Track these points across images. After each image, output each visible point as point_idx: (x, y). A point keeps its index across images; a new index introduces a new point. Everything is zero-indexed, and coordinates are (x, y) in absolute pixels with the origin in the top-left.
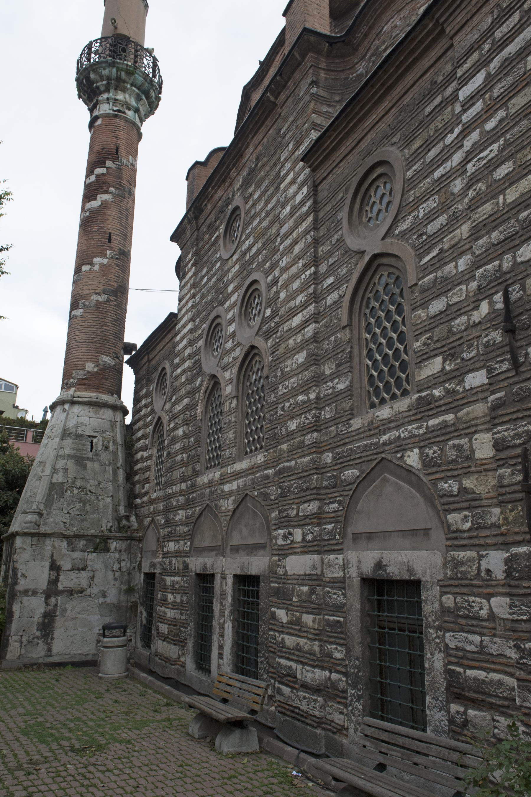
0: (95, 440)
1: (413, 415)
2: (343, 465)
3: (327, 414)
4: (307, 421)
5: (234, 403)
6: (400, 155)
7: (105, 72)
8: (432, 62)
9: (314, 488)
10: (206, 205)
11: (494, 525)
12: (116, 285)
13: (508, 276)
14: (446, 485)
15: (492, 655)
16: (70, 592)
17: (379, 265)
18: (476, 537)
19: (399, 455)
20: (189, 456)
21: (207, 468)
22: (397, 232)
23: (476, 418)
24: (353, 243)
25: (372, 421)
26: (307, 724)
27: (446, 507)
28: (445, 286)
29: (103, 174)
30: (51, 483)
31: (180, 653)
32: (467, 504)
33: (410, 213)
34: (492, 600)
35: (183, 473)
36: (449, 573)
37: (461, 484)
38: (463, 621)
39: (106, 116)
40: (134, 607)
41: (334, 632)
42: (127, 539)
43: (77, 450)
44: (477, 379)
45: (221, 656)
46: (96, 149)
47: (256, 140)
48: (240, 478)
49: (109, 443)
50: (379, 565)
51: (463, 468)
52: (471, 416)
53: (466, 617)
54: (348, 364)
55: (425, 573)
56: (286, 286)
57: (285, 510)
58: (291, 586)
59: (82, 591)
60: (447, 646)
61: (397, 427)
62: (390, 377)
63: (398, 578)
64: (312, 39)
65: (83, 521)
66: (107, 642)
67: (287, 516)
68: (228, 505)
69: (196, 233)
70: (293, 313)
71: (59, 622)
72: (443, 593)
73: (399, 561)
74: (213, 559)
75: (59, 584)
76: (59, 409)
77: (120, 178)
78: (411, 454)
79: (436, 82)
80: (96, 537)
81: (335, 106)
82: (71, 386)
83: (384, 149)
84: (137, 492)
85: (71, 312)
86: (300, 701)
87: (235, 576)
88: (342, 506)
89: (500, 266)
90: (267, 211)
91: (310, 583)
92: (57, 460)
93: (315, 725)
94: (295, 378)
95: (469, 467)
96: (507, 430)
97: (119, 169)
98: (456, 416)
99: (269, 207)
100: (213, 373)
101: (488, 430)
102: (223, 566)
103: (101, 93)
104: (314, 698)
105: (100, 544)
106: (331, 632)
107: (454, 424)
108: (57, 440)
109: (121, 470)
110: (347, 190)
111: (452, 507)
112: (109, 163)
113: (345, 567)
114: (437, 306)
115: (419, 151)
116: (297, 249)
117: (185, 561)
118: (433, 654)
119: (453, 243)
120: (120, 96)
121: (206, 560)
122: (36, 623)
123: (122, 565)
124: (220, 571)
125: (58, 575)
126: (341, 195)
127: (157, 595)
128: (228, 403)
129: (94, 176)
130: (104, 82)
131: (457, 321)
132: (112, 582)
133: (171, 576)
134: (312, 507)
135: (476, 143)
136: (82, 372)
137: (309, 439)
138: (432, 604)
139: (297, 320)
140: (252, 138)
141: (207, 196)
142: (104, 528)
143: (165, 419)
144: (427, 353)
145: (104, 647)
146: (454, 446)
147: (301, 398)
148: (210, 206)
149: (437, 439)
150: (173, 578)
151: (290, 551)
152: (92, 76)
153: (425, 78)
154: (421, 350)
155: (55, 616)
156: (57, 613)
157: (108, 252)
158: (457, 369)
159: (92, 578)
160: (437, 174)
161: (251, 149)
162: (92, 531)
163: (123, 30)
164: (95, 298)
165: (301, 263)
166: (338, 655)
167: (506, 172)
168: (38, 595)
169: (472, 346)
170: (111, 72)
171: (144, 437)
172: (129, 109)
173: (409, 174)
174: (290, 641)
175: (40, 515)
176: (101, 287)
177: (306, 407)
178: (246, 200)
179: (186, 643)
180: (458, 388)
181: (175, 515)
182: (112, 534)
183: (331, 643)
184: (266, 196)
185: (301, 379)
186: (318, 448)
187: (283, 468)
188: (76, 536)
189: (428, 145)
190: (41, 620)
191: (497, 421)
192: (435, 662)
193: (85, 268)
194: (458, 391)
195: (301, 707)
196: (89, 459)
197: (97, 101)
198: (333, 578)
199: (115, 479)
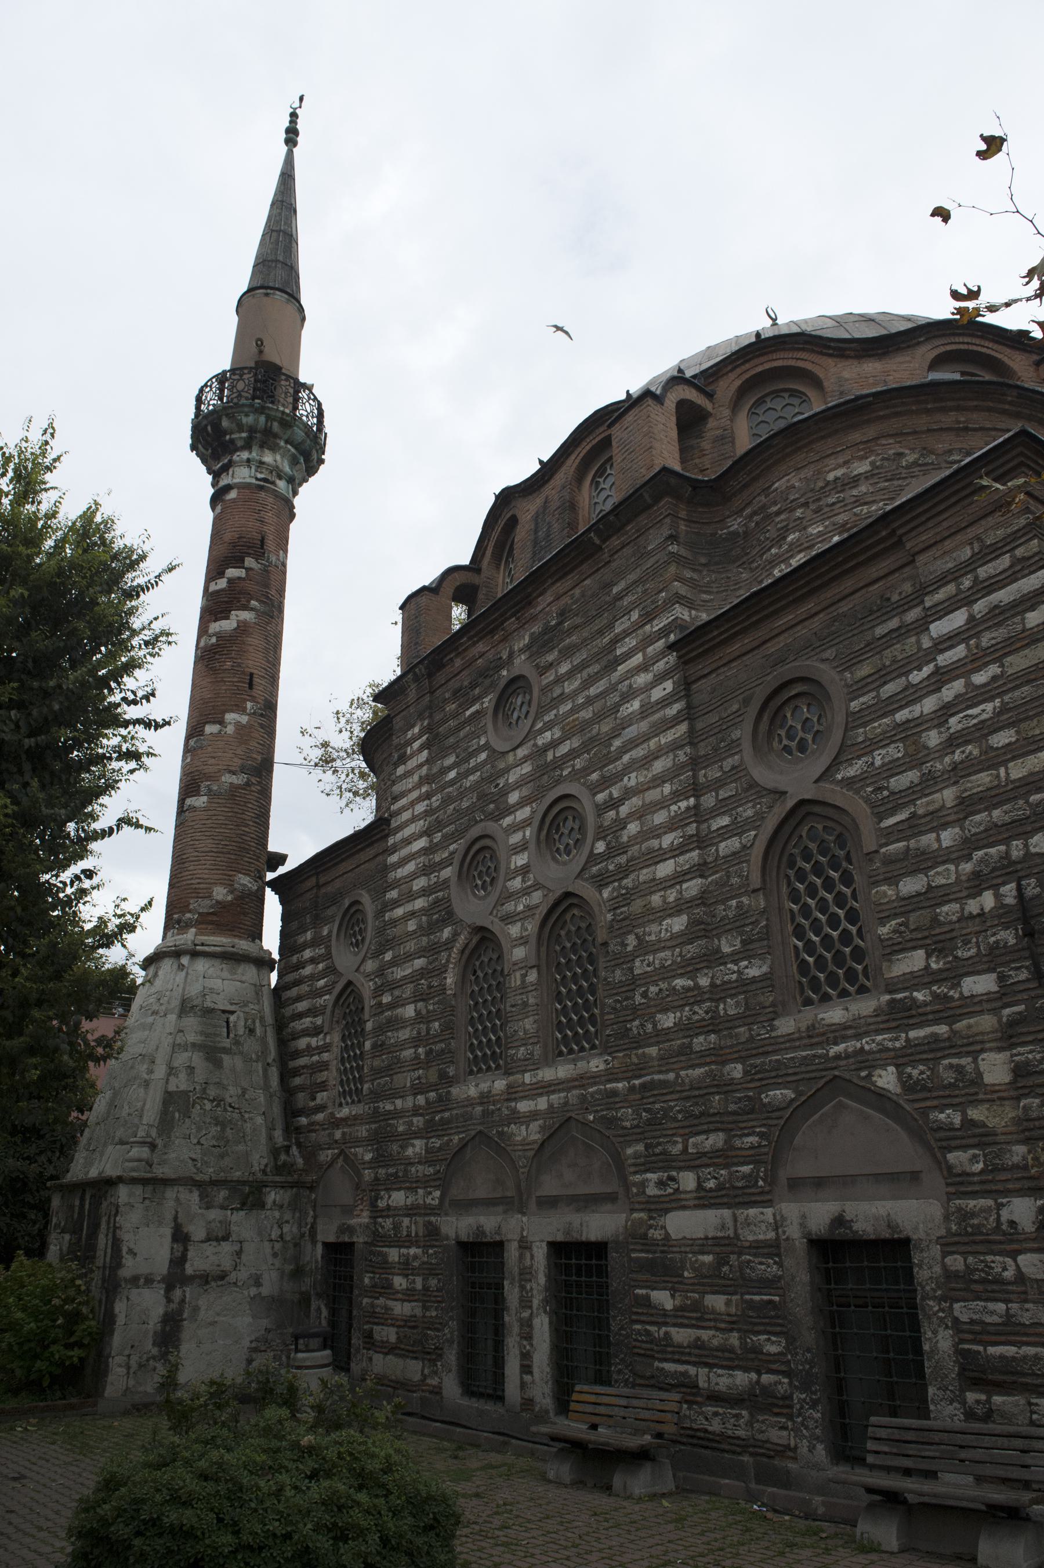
0: (232, 1018)
1: (883, 1022)
2: (764, 1082)
3: (730, 1007)
4: (696, 1017)
5: (532, 976)
6: (837, 678)
7: (248, 420)
8: (882, 573)
9: (715, 1114)
10: (451, 659)
11: (1016, 1167)
12: (259, 758)
13: (1019, 867)
14: (942, 1116)
15: (1024, 1325)
16: (205, 1279)
17: (808, 814)
18: (991, 1181)
19: (863, 1074)
20: (428, 1053)
21: (471, 1073)
22: (839, 777)
23: (982, 1033)
24: (764, 775)
25: (813, 1025)
26: (723, 1451)
27: (944, 1144)
28: (923, 862)
29: (239, 578)
30: (167, 1092)
31: (426, 1371)
32: (976, 1140)
33: (859, 757)
34: (1020, 1258)
35: (419, 1078)
36: (954, 1228)
37: (964, 1114)
38: (979, 1287)
39: (243, 487)
40: (305, 1300)
41: (770, 1317)
42: (292, 1185)
43: (207, 1035)
44: (980, 984)
45: (526, 1369)
46: (228, 537)
47: (560, 587)
48: (554, 1092)
49: (254, 1022)
50: (839, 1221)
51: (967, 1094)
52: (975, 1030)
53: (983, 1281)
54: (765, 943)
55: (916, 1228)
56: (639, 814)
57: (659, 1144)
58: (678, 1256)
59: (223, 1276)
60: (956, 1320)
61: (858, 1037)
62: (837, 965)
63: (872, 1237)
64: (673, 481)
65: (222, 1156)
66: (304, 1359)
67: (664, 1153)
68: (531, 1133)
69: (427, 698)
70: (659, 856)
71: (188, 1330)
72: (945, 1254)
73: (870, 1214)
74: (499, 1218)
75: (187, 1266)
76: (167, 966)
77: (267, 586)
78: (883, 1073)
79: (889, 599)
80: (244, 1183)
81: (700, 572)
82: (188, 925)
83: (807, 663)
84: (300, 1104)
85: (181, 802)
86: (707, 1419)
87: (552, 1245)
88: (767, 1139)
89: (1007, 853)
90: (588, 697)
91: (717, 1249)
92: (173, 1052)
93: (739, 1450)
94: (668, 953)
95: (976, 1094)
96: (1031, 1052)
97: (266, 571)
98: (951, 1030)
99: (593, 691)
100: (479, 923)
101: (1000, 1050)
102: (523, 1229)
103: (237, 450)
104: (734, 1412)
105: (249, 1196)
106: (759, 1317)
107: (949, 1038)
108: (172, 1017)
109: (274, 1069)
110: (746, 702)
111: (953, 1143)
112: (249, 562)
113: (777, 1225)
114: (911, 886)
115: (869, 680)
116: (659, 766)
117: (430, 1223)
118: (935, 1333)
119: (931, 808)
120: (268, 458)
121: (482, 1220)
122: (151, 1334)
123: (285, 1230)
124: (517, 1237)
125: (186, 1250)
126: (736, 707)
127: (362, 1281)
128: (518, 974)
129: (225, 580)
130: (244, 435)
131: (945, 908)
132: (270, 1260)
133: (400, 1247)
134: (715, 1140)
135: (960, 695)
136: (207, 902)
137: (699, 1042)
138: (930, 1268)
139: (666, 869)
140: (553, 584)
141: (457, 648)
142: (256, 1168)
143: (367, 988)
144: (900, 943)
145: (298, 1368)
146: (951, 1066)
147: (679, 983)
148: (458, 663)
149: (925, 1056)
150: (404, 1251)
151: (674, 1205)
152: (225, 423)
153: (871, 589)
154: (891, 938)
155: (183, 1320)
156: (185, 1315)
157: (249, 705)
158: (948, 970)
159: (239, 1253)
160: (901, 716)
161: (548, 597)
162: (238, 1174)
163: (272, 355)
164: (228, 779)
165: (667, 789)
166: (773, 1349)
167: (1007, 741)
168: (155, 1285)
169: (970, 942)
170: (257, 420)
171: (312, 1012)
172: (280, 478)
173: (855, 705)
174: (681, 1335)
175: (153, 1146)
176: (237, 762)
177: (693, 996)
178: (543, 670)
179: (440, 1355)
180: (951, 993)
181: (403, 1147)
182: (270, 1178)
183: (759, 1333)
184: (585, 674)
185: (680, 955)
186: (718, 1056)
187: (652, 1081)
188: (214, 1183)
189: (883, 676)
190: (159, 1327)
191: (1014, 1040)
192: (939, 1342)
193: (210, 729)
194: (952, 997)
195: (710, 1428)
196: (226, 1051)
197: (230, 461)
198: (757, 1241)
199: (266, 1087)
